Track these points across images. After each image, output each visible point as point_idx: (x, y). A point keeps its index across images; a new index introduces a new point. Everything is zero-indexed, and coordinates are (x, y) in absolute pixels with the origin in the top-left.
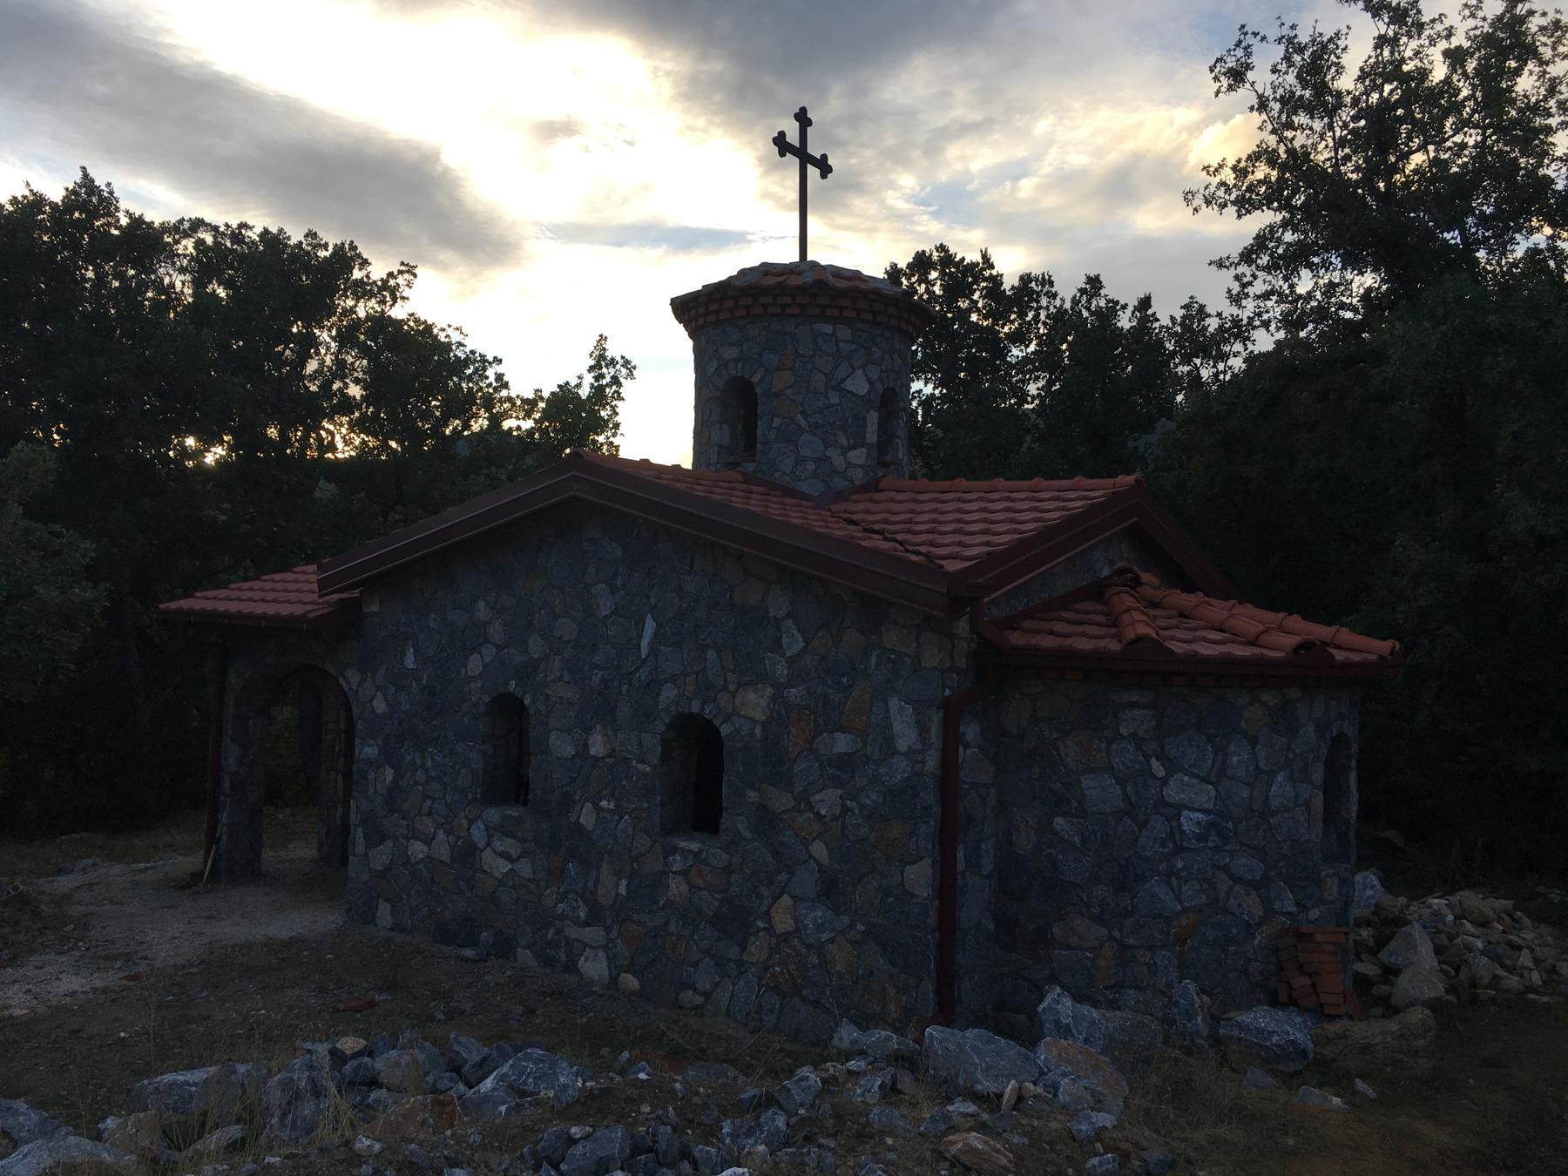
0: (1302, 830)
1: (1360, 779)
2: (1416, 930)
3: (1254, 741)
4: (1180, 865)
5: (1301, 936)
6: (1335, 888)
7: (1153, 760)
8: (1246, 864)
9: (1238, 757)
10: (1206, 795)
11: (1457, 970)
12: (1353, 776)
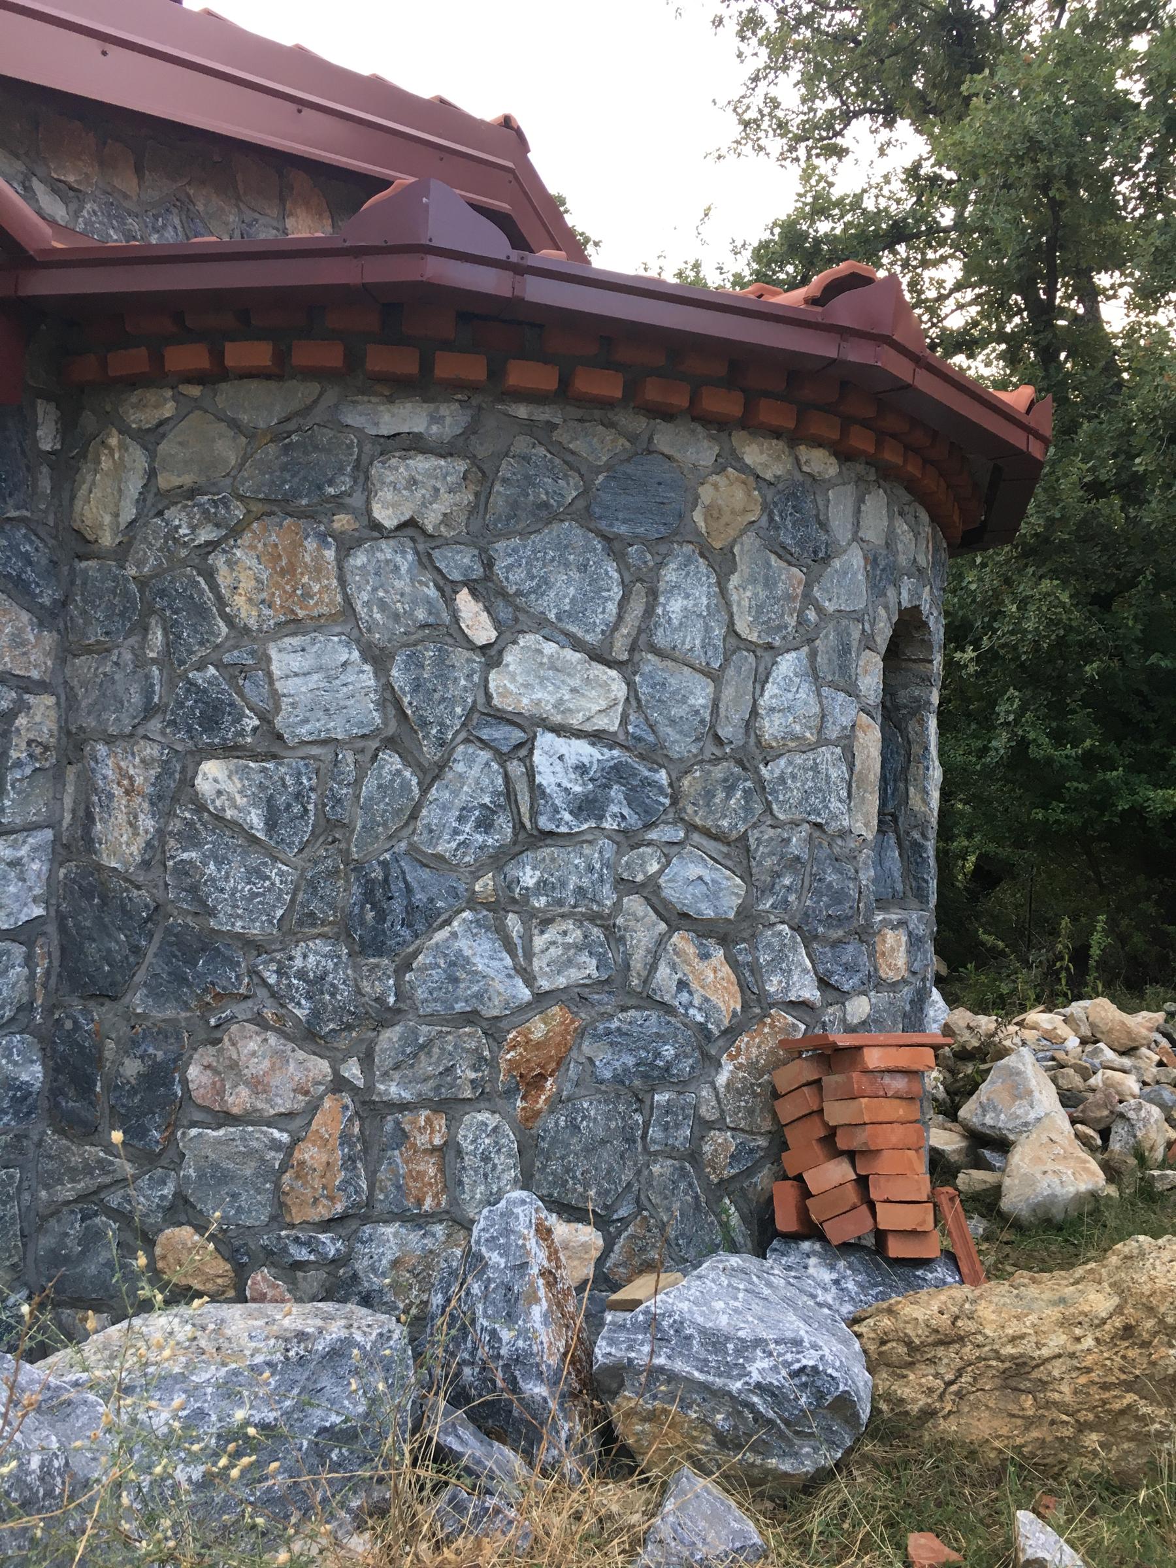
0: (835, 805)
1: (940, 725)
2: (1025, 1063)
3: (722, 564)
4: (529, 878)
5: (834, 1058)
6: (901, 960)
7: (464, 599)
8: (699, 880)
9: (685, 600)
10: (599, 696)
11: (1105, 1134)
12: (933, 723)
